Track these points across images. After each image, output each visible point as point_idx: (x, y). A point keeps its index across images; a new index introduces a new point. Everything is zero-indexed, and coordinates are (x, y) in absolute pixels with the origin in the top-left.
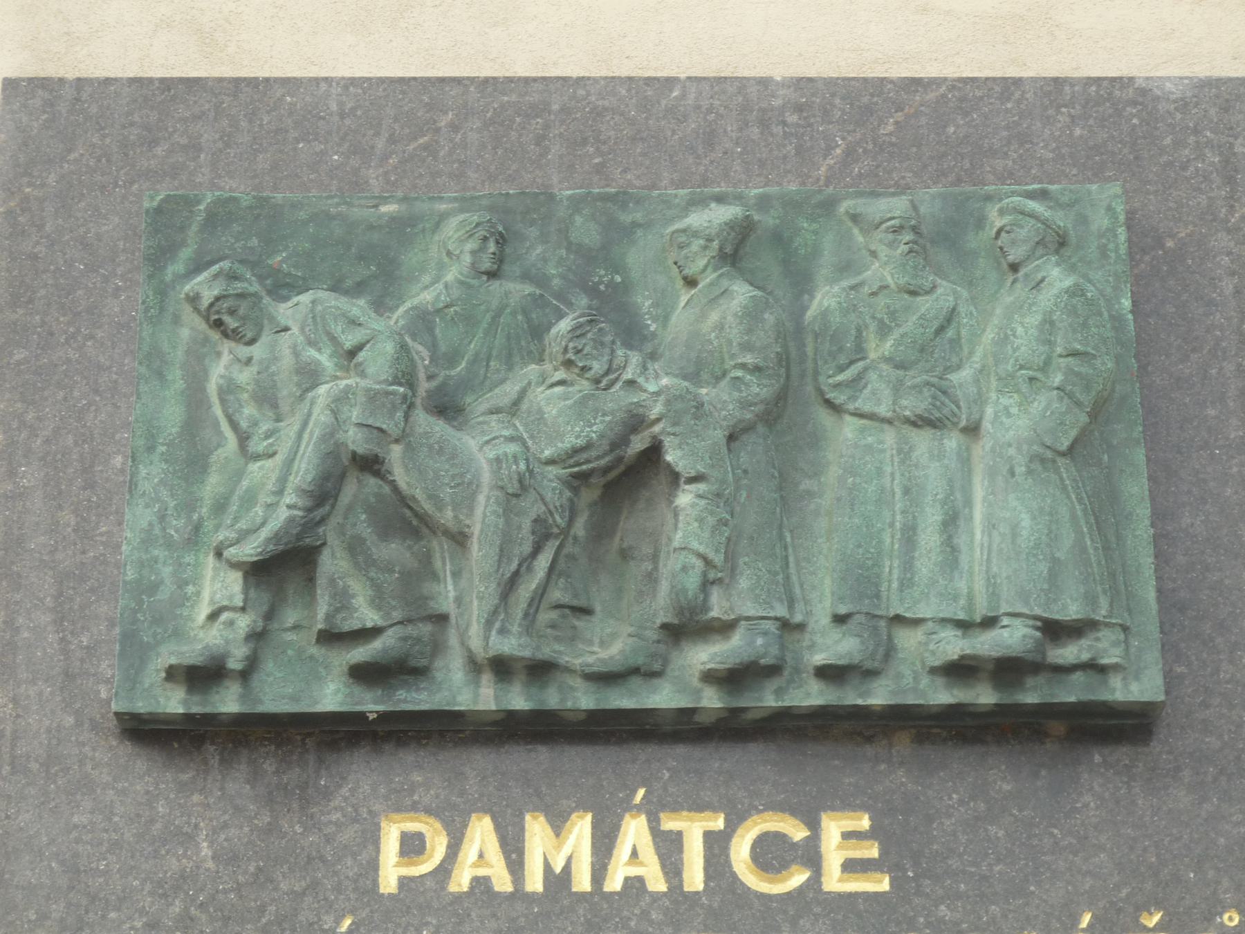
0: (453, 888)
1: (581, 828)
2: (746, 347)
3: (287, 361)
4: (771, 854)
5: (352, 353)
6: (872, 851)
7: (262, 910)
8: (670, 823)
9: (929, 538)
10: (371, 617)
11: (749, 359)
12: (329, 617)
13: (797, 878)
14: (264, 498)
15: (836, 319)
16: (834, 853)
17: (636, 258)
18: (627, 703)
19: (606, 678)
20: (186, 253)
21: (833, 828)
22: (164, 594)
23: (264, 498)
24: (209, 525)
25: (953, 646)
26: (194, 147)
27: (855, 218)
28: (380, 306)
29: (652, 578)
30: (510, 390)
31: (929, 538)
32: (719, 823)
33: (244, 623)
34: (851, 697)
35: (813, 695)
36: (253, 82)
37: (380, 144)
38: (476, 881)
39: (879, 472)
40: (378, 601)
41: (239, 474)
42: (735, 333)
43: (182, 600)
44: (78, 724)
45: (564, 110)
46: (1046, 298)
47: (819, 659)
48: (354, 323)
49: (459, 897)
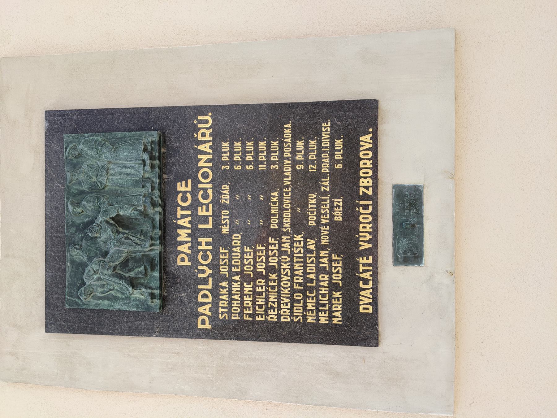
0: (190, 253)
1: (179, 231)
2: (94, 202)
3: (96, 283)
4: (184, 199)
5: (95, 272)
6: (184, 182)
7: (194, 285)
8: (179, 216)
9: (129, 171)
10: (142, 268)
11: (96, 202)
12: (143, 275)
13: (188, 195)
14: (121, 286)
15: (89, 186)
16: (184, 189)
17: (78, 221)
18: (158, 224)
19: (154, 227)
20: (77, 300)
21: (179, 189)
22: (138, 303)
23: (121, 286)
24: (126, 296)
25: (148, 168)
26: (58, 299)
27: (70, 182)
28: (87, 266)
29: (136, 219)
30: (102, 243)
31: (129, 171)
32: (179, 208)
33: (143, 290)
34: (157, 185)
35: (157, 192)
36: (46, 288)
37: (57, 266)
38: (189, 249)
39: (116, 179)
40: (140, 267)
41: (117, 290)
42: (91, 204)
43: (140, 300)
44: (162, 317)
45: (51, 233)
46: (85, 149)
47: (150, 191)
48: (89, 271)
49: (192, 252)
